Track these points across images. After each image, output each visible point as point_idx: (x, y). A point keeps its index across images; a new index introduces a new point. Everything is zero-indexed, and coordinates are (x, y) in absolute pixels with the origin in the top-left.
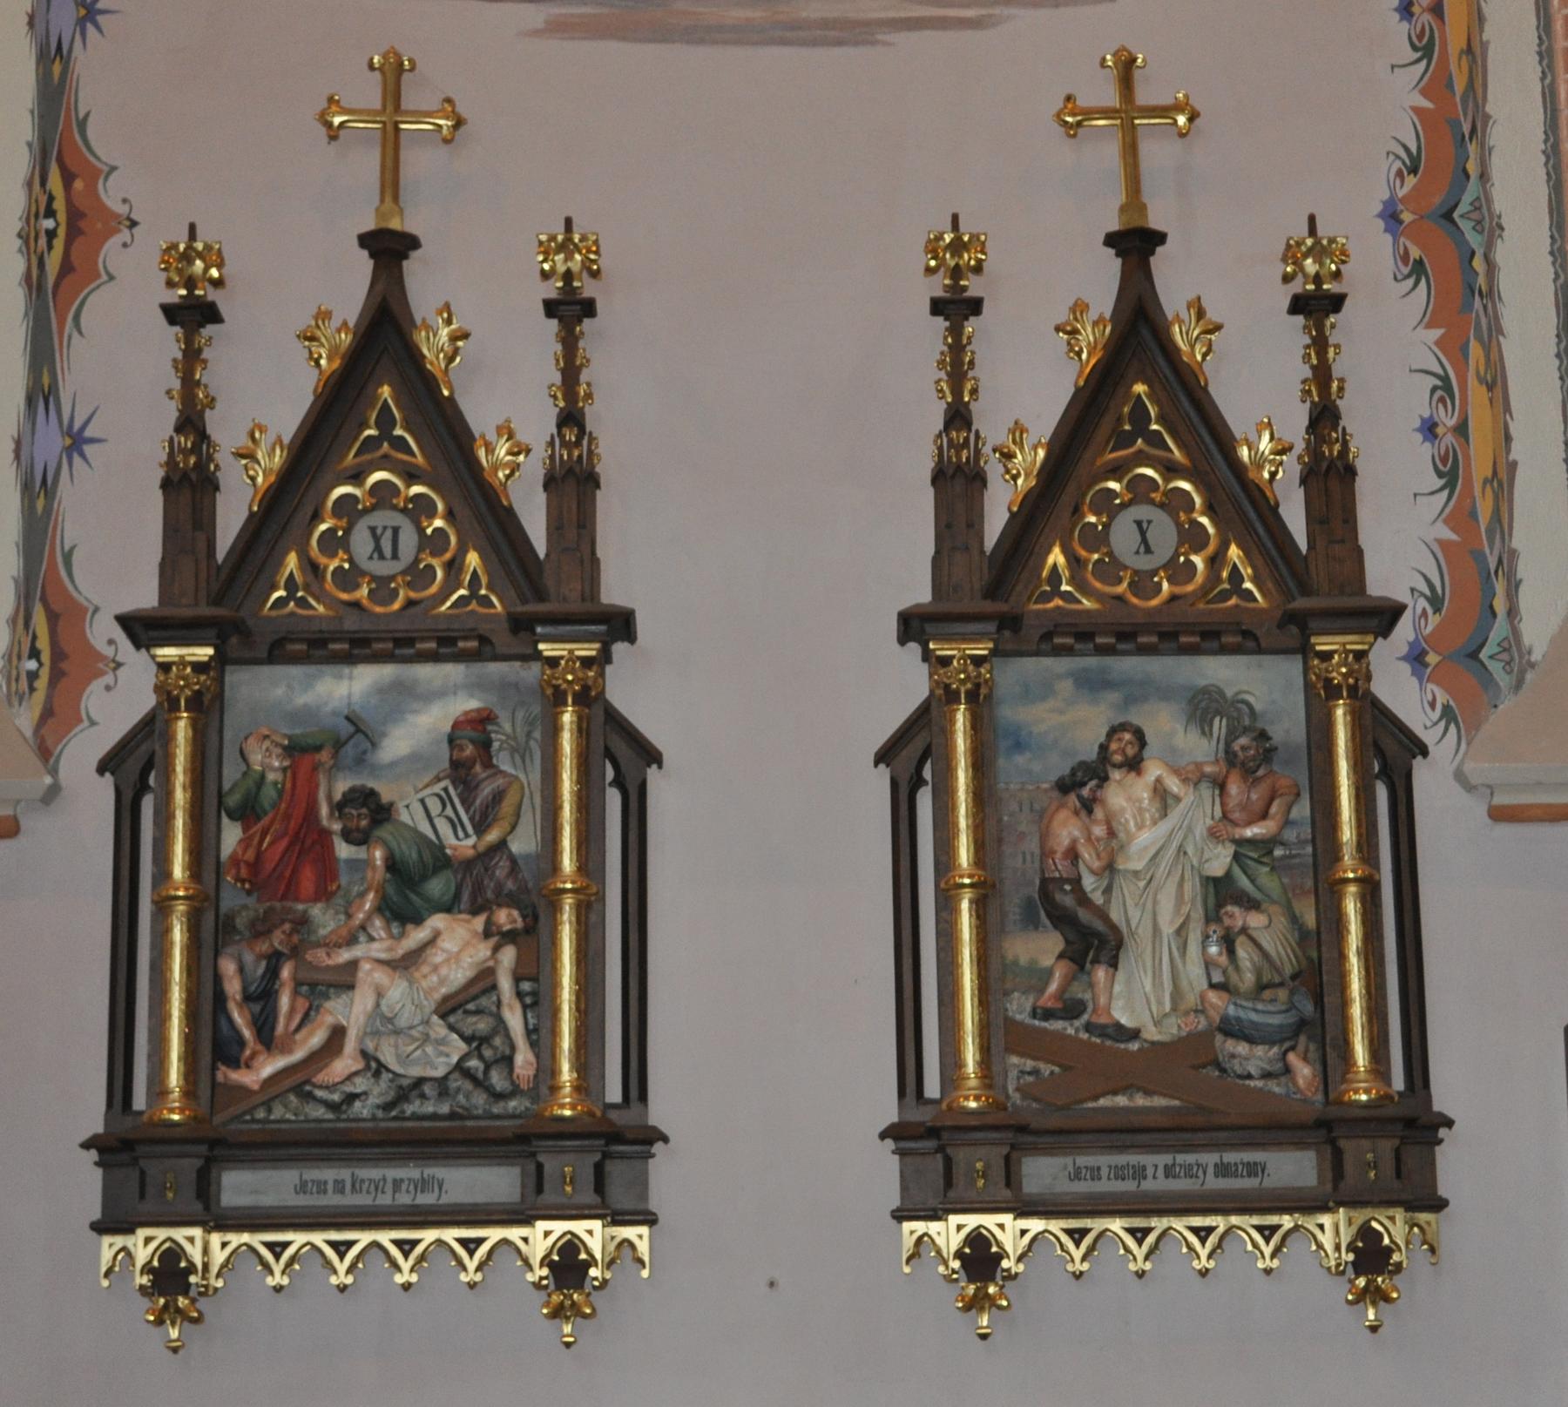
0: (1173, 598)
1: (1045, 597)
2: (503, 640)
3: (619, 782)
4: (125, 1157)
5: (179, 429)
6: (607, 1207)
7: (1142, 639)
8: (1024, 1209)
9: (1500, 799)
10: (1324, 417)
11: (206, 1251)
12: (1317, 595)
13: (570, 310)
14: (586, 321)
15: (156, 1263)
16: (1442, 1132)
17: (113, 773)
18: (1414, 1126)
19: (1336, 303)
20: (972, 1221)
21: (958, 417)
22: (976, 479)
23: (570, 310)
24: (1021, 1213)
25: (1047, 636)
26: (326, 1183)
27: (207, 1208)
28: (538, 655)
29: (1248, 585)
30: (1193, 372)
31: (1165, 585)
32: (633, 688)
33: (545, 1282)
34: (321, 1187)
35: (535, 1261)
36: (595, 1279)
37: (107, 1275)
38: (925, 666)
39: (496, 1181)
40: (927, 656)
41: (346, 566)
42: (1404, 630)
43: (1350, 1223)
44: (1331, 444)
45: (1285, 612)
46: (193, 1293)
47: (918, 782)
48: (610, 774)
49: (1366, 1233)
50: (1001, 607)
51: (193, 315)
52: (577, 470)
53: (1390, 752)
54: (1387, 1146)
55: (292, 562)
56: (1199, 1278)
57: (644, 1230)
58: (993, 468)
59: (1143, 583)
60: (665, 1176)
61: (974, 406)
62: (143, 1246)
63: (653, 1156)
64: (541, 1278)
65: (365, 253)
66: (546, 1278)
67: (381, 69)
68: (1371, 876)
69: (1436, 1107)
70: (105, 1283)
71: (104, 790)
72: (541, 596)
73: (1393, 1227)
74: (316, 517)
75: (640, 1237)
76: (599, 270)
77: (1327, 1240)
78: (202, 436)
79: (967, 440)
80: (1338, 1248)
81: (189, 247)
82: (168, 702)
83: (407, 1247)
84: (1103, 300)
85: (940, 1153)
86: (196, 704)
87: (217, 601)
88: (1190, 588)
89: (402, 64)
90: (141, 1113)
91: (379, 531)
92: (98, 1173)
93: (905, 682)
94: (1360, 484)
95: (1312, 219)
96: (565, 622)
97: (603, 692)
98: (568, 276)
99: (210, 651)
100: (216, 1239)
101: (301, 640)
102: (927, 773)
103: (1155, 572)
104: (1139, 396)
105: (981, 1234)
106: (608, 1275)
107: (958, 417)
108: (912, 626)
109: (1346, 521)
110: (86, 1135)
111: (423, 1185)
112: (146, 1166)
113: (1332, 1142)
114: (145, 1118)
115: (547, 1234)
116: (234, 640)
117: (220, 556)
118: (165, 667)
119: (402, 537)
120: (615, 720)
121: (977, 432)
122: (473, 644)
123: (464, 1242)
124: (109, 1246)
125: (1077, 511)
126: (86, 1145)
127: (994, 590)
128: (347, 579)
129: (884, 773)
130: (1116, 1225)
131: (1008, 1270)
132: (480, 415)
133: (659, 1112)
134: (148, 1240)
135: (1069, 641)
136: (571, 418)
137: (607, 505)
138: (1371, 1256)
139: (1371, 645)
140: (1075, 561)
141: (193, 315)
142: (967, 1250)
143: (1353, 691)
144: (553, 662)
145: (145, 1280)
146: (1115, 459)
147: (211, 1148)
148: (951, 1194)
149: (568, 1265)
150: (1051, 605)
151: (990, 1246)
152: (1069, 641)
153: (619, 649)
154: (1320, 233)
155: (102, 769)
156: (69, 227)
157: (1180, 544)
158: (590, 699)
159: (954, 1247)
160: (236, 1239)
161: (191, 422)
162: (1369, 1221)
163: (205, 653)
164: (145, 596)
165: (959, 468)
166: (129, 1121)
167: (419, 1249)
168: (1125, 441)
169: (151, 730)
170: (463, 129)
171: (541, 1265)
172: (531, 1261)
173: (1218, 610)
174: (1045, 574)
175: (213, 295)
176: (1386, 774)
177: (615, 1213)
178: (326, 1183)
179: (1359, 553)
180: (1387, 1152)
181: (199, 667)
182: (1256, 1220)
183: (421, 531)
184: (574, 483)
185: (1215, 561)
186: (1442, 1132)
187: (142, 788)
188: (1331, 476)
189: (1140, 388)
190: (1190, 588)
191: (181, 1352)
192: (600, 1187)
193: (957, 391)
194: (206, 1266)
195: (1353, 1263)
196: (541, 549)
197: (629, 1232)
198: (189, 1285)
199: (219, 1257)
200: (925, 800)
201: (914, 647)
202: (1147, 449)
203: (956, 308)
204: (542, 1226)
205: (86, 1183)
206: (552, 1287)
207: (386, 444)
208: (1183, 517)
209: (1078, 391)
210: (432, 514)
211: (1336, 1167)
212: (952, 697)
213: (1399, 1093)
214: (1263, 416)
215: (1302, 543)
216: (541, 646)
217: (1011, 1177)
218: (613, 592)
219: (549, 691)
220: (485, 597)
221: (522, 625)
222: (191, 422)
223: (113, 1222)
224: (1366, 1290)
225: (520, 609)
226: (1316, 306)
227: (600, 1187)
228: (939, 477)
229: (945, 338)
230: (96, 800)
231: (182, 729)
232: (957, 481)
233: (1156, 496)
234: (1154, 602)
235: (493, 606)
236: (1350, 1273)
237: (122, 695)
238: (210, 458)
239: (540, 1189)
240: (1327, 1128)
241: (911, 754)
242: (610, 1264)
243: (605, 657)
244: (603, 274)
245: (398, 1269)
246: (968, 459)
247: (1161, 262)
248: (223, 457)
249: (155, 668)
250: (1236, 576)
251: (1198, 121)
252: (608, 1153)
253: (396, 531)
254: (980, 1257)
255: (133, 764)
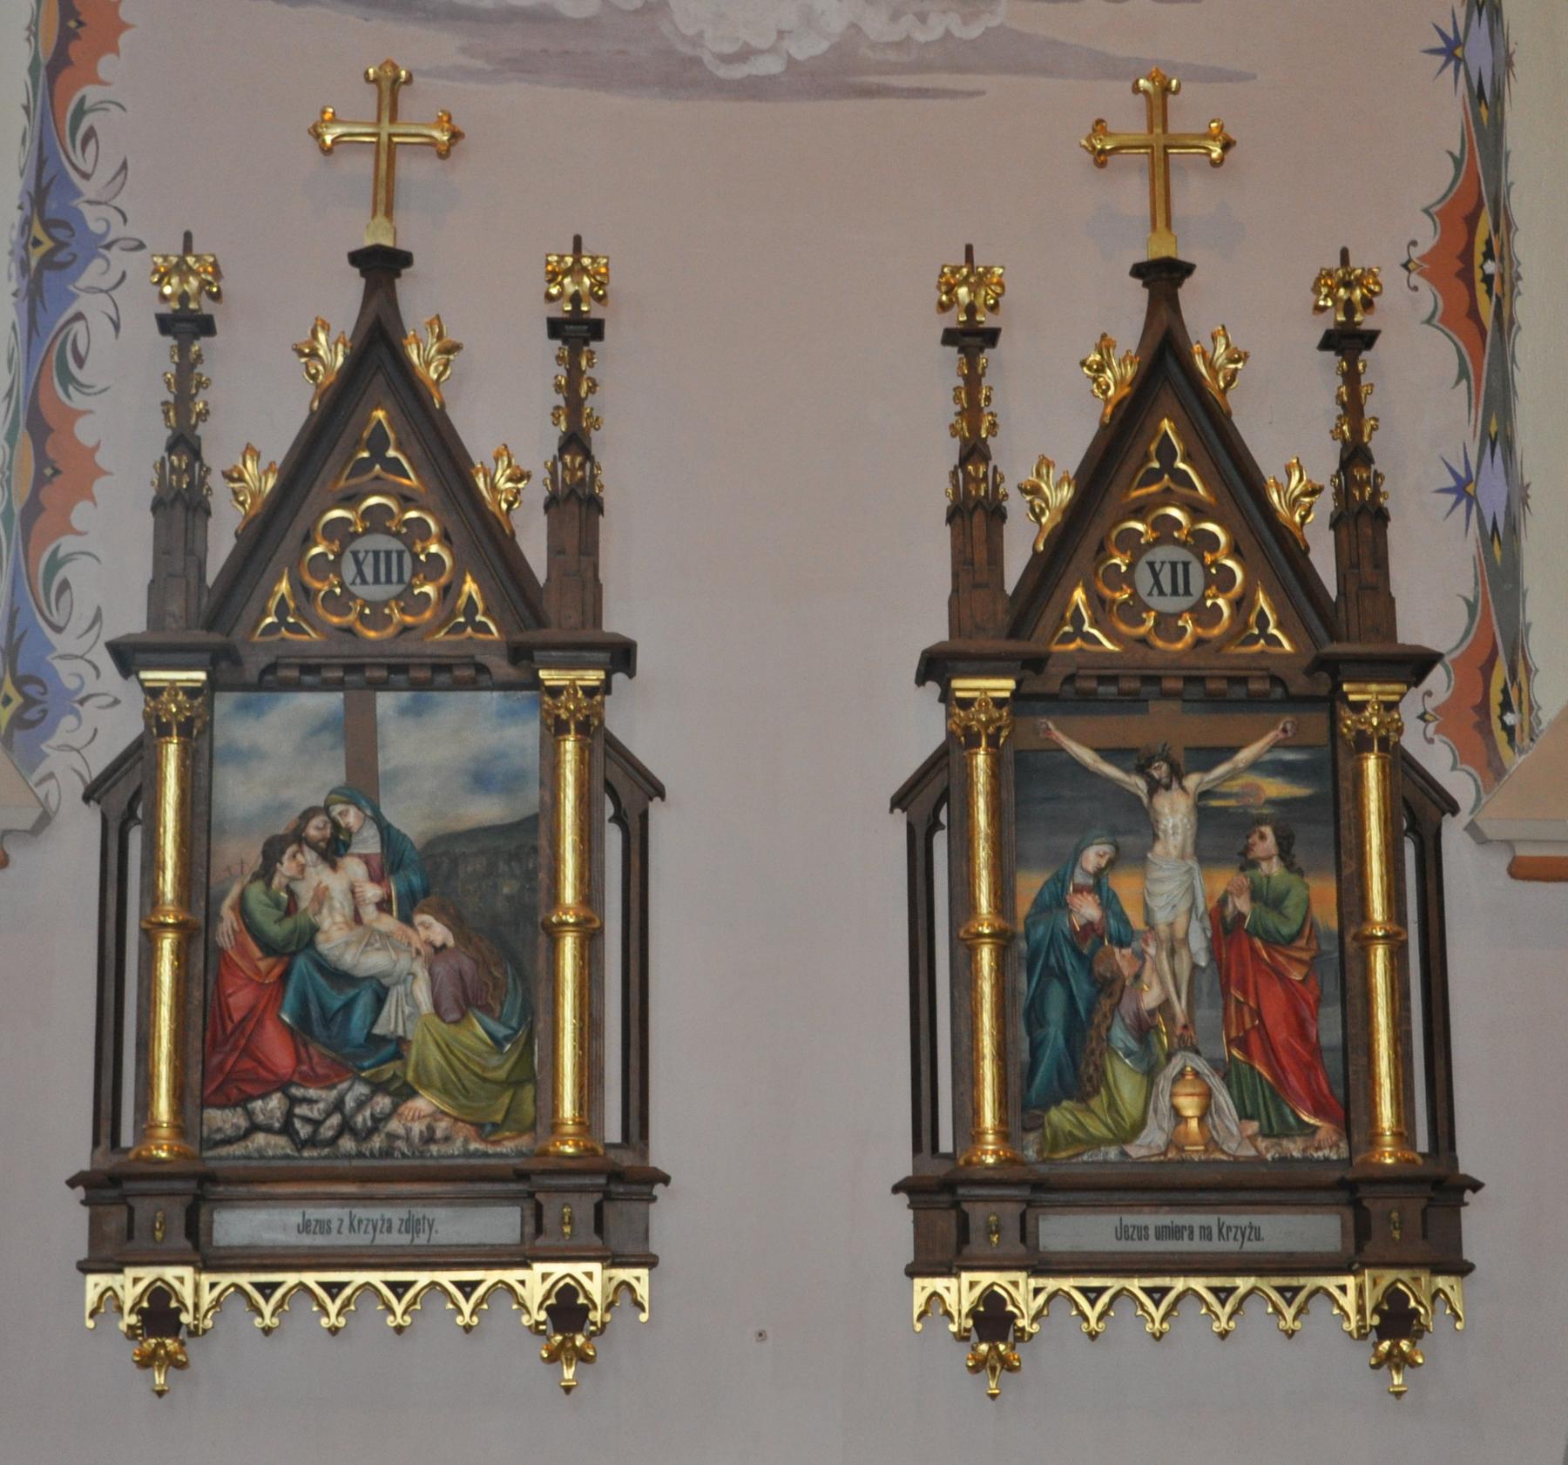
0: (1199, 642)
1: (1068, 638)
2: (502, 668)
3: (618, 818)
4: (113, 1193)
5: (171, 448)
6: (607, 1249)
7: (457, 673)
8: (1040, 1267)
9: (1524, 851)
10: (1355, 455)
11: (197, 1287)
12: (1350, 639)
13: (576, 332)
14: (204, 340)
15: (145, 1304)
16: (1468, 1195)
17: (98, 802)
18: (1441, 1188)
19: (991, 337)
20: (986, 1278)
21: (974, 451)
22: (997, 514)
23: (576, 332)
24: (1035, 1272)
25: (272, 668)
26: (1146, 1228)
27: (196, 1247)
28: (537, 684)
29: (1272, 630)
30: (499, 523)
31: (1190, 627)
32: (636, 721)
33: (542, 1327)
34: (1142, 1233)
35: (533, 1305)
36: (594, 1324)
37: (93, 1314)
38: (942, 707)
39: (501, 1223)
40: (946, 696)
41: (338, 590)
42: (1437, 679)
43: (1375, 1283)
44: (1362, 485)
45: (1317, 657)
46: (182, 1335)
47: (934, 826)
48: (610, 810)
49: (1394, 1297)
50: (215, 638)
51: (187, 325)
52: (580, 492)
53: (1420, 809)
54: (1415, 1207)
55: (284, 587)
56: (1218, 1340)
57: (643, 1273)
58: (1016, 505)
59: (1167, 625)
60: (668, 1218)
61: (991, 442)
62: (130, 1285)
63: (654, 1199)
64: (538, 1323)
65: (357, 271)
66: (544, 1323)
67: (376, 81)
68: (1398, 934)
69: (1462, 1170)
70: (90, 1324)
71: (90, 819)
72: (541, 622)
73: (1418, 1288)
74: (308, 540)
75: (638, 1279)
76: (605, 296)
77: (1349, 1302)
78: (196, 454)
79: (985, 474)
80: (1361, 1310)
81: (182, 260)
82: (157, 728)
83: (1092, 1296)
84: (1129, 331)
85: (949, 1211)
86: (185, 730)
87: (210, 625)
88: (1216, 631)
89: (398, 77)
90: (127, 1150)
91: (1157, 567)
92: (84, 1213)
93: (920, 728)
94: (1393, 531)
95: (969, 250)
96: (575, 652)
97: (602, 722)
98: (576, 299)
99: (201, 675)
100: (206, 1279)
101: (422, 665)
102: (943, 817)
103: (1179, 616)
104: (379, 422)
105: (567, 1285)
106: (608, 1318)
107: (974, 451)
108: (935, 667)
109: (1376, 566)
110: (73, 1171)
111: (1175, 1232)
112: (138, 1203)
113: (1356, 1204)
114: (132, 1155)
115: (972, 1285)
116: (224, 665)
117: (211, 578)
118: (153, 693)
119: (1191, 568)
120: (614, 747)
121: (995, 468)
122: (468, 673)
123: (260, 1287)
124: (95, 1284)
125: (1102, 550)
126: (72, 1183)
127: (1019, 626)
128: (338, 603)
129: (900, 818)
130: (1199, 1284)
131: (1022, 1329)
132: (478, 440)
133: (660, 1155)
134: (136, 1281)
135: (382, 673)
136: (576, 442)
137: (610, 529)
138: (1396, 1319)
139: (1402, 695)
140: (303, 592)
141: (187, 325)
142: (1386, 1307)
143: (1384, 744)
144: (555, 692)
145: (133, 1319)
146: (1138, 498)
147: (200, 1185)
148: (540, 1242)
149: (567, 1309)
150: (1072, 646)
151: (577, 1295)
152: (294, 673)
153: (619, 678)
154: (1352, 263)
155: (900, 801)
156: (56, 242)
157: (1207, 587)
158: (592, 731)
159: (965, 1310)
160: (225, 1280)
161: (184, 442)
162: (1394, 1283)
163: (1003, 686)
164: (131, 620)
165: (979, 503)
166: (115, 1159)
167: (348, 1291)
168: (1154, 477)
169: (137, 762)
170: (462, 143)
171: (131, 1311)
172: (528, 1304)
173: (1244, 656)
174: (1068, 615)
175: (208, 307)
176: (1414, 829)
177: (615, 1256)
178: (1146, 1228)
179: (1392, 601)
180: (1409, 1215)
181: (192, 693)
182: (1149, 1282)
183: (415, 556)
184: (577, 505)
185: (1241, 604)
186: (1468, 1195)
187: (129, 818)
188: (1362, 518)
189: (380, 414)
190: (1216, 631)
191: (166, 1397)
192: (599, 1227)
193: (974, 429)
194: (196, 1307)
195: (1377, 1328)
196: (541, 574)
197: (1442, 1282)
198: (180, 1324)
199: (207, 1298)
200: (940, 842)
201: (933, 688)
202: (1172, 486)
203: (972, 339)
204: (539, 1268)
205: (71, 1221)
206: (551, 1332)
207: (378, 467)
208: (1209, 558)
209: (1104, 427)
210: (426, 535)
211: (1361, 1231)
212: (972, 742)
213: (1423, 1155)
214: (1293, 453)
215: (1333, 592)
216: (543, 674)
217: (1026, 1234)
218: (616, 621)
219: (550, 721)
220: (465, 614)
221: (520, 654)
222: (184, 442)
223: (101, 1260)
224: (1389, 1354)
225: (518, 637)
226: (1349, 342)
227: (599, 1227)
228: (956, 514)
229: (960, 368)
230: (81, 831)
231: (172, 750)
232: (975, 514)
233: (392, 525)
234: (1180, 646)
235: (490, 632)
236: (1373, 1336)
237: (105, 721)
238: (202, 481)
239: (539, 1230)
240: (1352, 1191)
241: (929, 797)
242: (609, 1307)
243: (606, 688)
244: (610, 298)
245: (391, 1311)
246: (986, 492)
247: (1188, 293)
248: (215, 481)
249: (142, 696)
250: (1262, 620)
251: (1232, 152)
252: (609, 1195)
253: (1186, 565)
254: (992, 1318)
255: (122, 794)
